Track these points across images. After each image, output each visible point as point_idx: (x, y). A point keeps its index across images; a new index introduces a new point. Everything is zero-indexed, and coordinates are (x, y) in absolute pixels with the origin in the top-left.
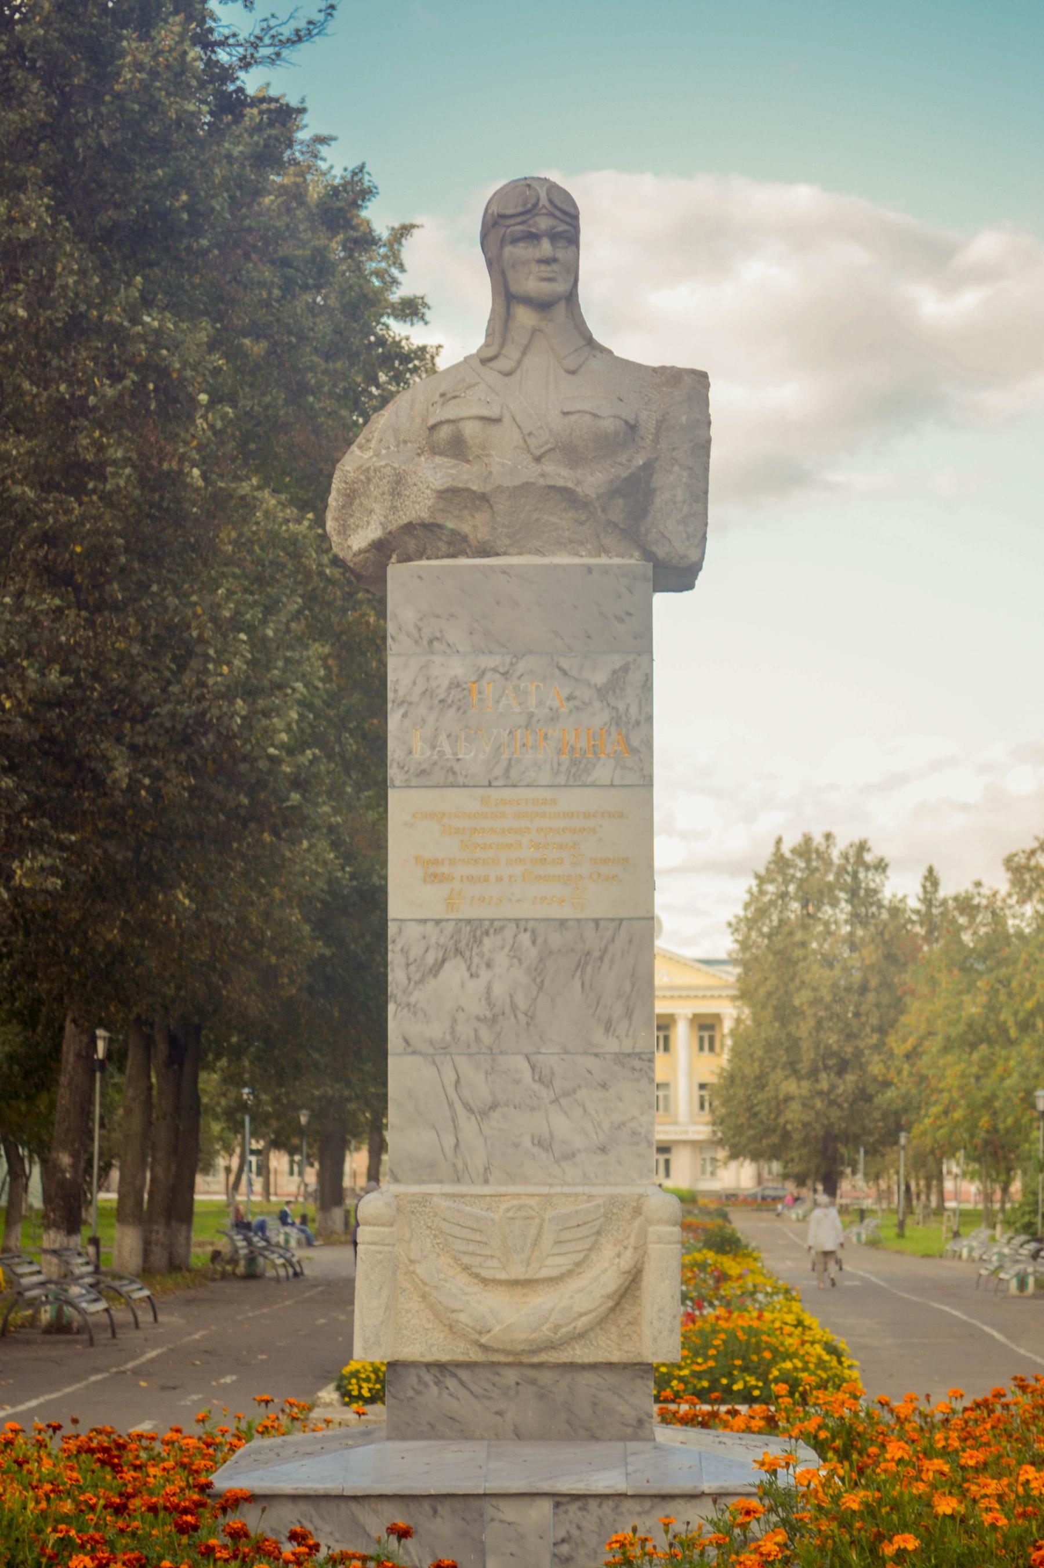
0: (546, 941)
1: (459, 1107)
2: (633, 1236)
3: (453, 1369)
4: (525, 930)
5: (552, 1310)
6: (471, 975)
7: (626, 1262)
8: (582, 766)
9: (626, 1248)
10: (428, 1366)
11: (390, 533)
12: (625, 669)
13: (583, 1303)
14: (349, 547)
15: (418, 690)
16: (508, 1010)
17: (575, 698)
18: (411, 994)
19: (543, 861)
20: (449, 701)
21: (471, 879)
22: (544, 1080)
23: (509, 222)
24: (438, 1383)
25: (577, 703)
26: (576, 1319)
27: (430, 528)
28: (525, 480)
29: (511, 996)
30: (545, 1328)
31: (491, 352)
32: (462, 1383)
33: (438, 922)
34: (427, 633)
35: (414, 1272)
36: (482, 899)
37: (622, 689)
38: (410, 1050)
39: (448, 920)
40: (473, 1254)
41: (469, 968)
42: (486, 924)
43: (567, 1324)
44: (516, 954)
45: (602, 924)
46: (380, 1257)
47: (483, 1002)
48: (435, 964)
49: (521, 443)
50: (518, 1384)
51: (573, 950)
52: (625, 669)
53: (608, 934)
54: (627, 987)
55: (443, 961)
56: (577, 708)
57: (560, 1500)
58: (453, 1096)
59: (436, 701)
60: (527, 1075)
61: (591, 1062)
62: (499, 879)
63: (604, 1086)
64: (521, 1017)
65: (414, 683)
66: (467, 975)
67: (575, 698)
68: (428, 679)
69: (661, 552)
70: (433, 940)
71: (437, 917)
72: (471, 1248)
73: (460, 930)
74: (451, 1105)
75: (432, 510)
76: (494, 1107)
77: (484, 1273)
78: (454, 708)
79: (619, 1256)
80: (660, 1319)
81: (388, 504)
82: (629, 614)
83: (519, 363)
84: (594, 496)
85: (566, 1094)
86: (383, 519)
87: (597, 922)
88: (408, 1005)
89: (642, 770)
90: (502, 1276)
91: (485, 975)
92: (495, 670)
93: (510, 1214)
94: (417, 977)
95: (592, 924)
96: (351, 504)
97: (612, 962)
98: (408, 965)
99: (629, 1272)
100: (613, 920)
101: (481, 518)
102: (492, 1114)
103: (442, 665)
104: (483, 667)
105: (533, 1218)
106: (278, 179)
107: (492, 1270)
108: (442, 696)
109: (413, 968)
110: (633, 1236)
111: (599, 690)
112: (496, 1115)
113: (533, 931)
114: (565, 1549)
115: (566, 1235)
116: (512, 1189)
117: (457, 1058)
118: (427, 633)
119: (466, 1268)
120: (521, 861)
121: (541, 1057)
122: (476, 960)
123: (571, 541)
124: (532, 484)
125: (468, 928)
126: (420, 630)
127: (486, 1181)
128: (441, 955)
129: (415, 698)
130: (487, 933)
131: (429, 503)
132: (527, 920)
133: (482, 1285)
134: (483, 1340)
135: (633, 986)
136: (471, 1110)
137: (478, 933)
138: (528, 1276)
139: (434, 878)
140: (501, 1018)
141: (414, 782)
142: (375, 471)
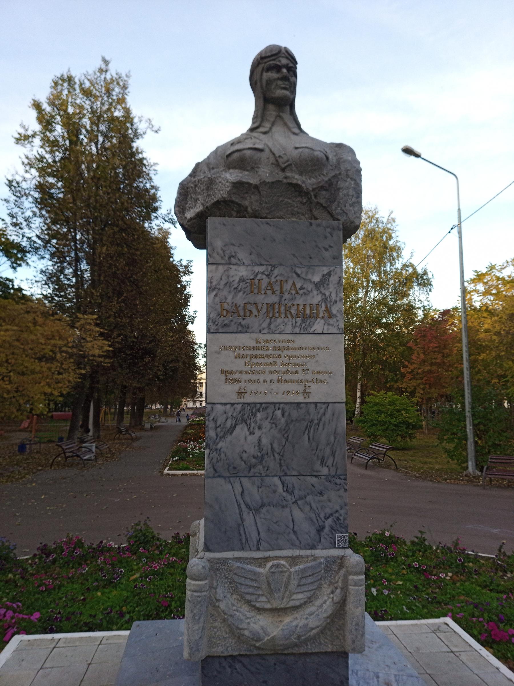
0: (289, 414)
1: (243, 506)
2: (340, 581)
3: (239, 658)
4: (279, 409)
5: (297, 626)
6: (250, 433)
7: (337, 596)
8: (307, 323)
9: (336, 588)
10: (225, 657)
11: (207, 207)
12: (329, 274)
13: (313, 622)
14: (186, 218)
15: (223, 282)
16: (270, 452)
17: (304, 289)
18: (218, 444)
19: (288, 372)
20: (239, 289)
21: (250, 381)
22: (289, 491)
23: (265, 61)
25: (304, 291)
26: (310, 631)
28: (277, 179)
29: (271, 444)
30: (293, 637)
31: (256, 125)
32: (244, 666)
33: (233, 404)
34: (228, 252)
35: (218, 606)
37: (328, 285)
38: (216, 475)
39: (238, 403)
40: (252, 594)
41: (249, 430)
42: (258, 405)
43: (305, 635)
44: (274, 422)
45: (319, 405)
46: (200, 599)
47: (257, 448)
48: (231, 427)
49: (274, 162)
50: (275, 664)
51: (304, 419)
52: (329, 274)
53: (322, 411)
54: (332, 439)
56: (305, 294)
59: (232, 289)
63: (321, 494)
64: (277, 455)
65: (221, 279)
66: (248, 433)
67: (304, 289)
68: (228, 277)
70: (230, 414)
71: (232, 402)
72: (251, 590)
73: (244, 409)
74: (239, 506)
76: (262, 506)
77: (258, 605)
78: (242, 292)
79: (332, 592)
80: (356, 630)
81: (205, 194)
82: (331, 247)
83: (270, 129)
84: (311, 189)
86: (202, 202)
87: (316, 404)
88: (216, 449)
89: (338, 326)
90: (268, 606)
91: (258, 433)
92: (263, 273)
93: (272, 570)
94: (222, 434)
95: (313, 406)
96: (186, 198)
97: (324, 425)
98: (216, 428)
99: (338, 603)
100: (324, 403)
102: (261, 510)
103: (236, 270)
104: (257, 271)
105: (285, 572)
106: (190, 405)
107: (262, 602)
108: (235, 286)
109: (219, 430)
110: (340, 581)
112: (264, 510)
113: (283, 409)
115: (304, 581)
116: (273, 553)
117: (242, 479)
118: (228, 252)
119: (248, 602)
120: (276, 372)
121: (287, 478)
122: (253, 425)
123: (298, 213)
124: (281, 181)
125: (249, 408)
126: (224, 251)
127: (258, 549)
128: (234, 422)
129: (221, 287)
130: (258, 410)
131: (228, 189)
132: (280, 403)
133: (256, 611)
134: (258, 645)
135: (335, 439)
136: (250, 509)
137: (254, 410)
138: (282, 606)
140: (266, 456)
141: (220, 331)
142: (198, 181)
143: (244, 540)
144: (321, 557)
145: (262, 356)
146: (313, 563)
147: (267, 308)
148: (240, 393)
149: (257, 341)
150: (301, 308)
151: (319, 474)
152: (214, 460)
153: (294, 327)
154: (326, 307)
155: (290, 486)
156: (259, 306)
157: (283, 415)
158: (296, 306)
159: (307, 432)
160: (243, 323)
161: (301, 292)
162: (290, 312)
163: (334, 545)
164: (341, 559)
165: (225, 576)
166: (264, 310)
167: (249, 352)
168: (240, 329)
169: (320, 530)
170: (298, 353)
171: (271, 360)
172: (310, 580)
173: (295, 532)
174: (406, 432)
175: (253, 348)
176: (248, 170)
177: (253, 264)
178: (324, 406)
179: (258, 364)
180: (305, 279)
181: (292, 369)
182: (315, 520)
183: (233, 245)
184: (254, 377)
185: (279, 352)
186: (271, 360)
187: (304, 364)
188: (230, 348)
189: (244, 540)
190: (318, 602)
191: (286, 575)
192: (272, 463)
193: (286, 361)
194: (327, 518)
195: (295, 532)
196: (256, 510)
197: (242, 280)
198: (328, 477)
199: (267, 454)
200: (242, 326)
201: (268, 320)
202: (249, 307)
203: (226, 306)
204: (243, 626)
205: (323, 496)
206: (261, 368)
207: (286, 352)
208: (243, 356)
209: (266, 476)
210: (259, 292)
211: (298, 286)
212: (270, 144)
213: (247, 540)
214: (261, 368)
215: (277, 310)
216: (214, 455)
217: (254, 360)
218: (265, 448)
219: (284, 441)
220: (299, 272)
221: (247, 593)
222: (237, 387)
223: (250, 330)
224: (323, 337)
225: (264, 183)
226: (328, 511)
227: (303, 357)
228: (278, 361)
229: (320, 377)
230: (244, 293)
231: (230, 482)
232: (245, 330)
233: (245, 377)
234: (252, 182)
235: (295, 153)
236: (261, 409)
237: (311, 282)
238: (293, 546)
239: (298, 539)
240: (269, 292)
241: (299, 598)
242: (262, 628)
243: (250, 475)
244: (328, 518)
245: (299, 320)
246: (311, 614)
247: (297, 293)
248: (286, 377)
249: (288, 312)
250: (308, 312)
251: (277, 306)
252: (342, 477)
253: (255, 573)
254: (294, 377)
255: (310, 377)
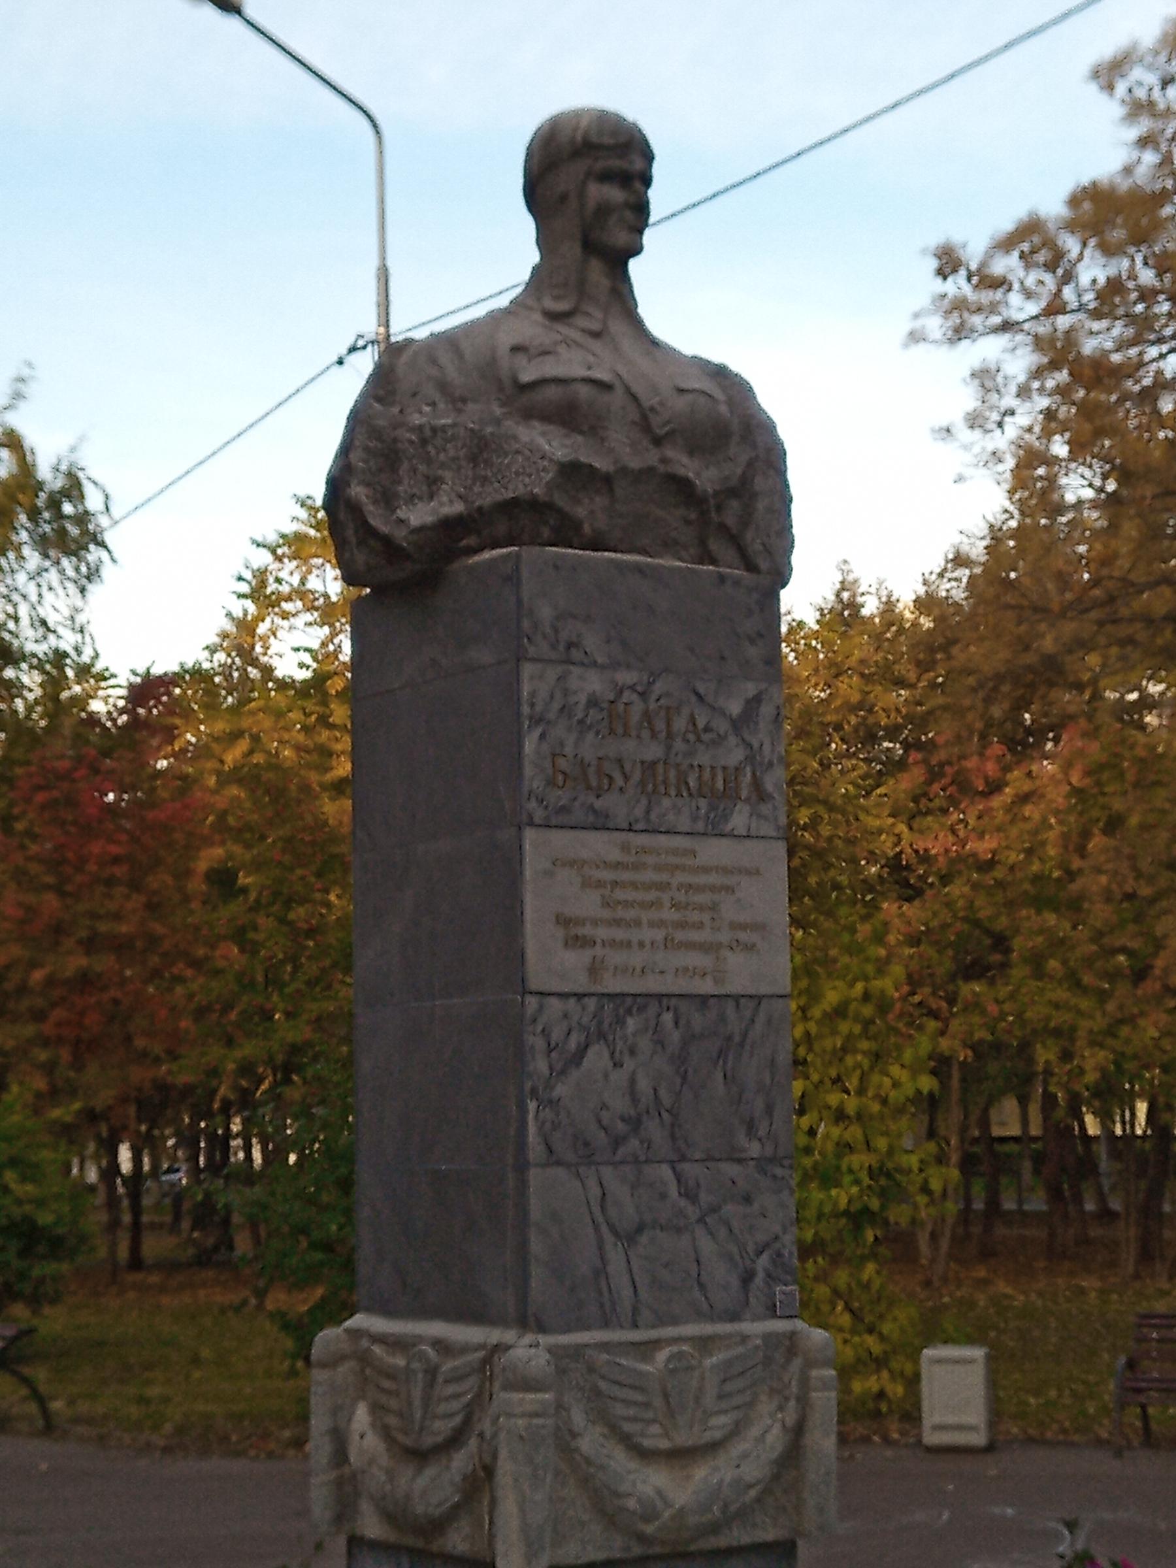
2: (794, 1383)
4: (668, 1009)
6: (615, 1065)
7: (790, 1416)
9: (787, 1399)
12: (757, 699)
15: (556, 706)
19: (682, 925)
21: (613, 944)
22: (689, 1194)
27: (534, 506)
29: (655, 1090)
33: (580, 996)
34: (564, 636)
41: (612, 1054)
45: (743, 1001)
53: (748, 1014)
55: (587, 1046)
58: (600, 1219)
62: (641, 945)
64: (665, 1115)
65: (552, 697)
70: (576, 1018)
71: (581, 990)
75: (549, 486)
76: (640, 1229)
77: (647, 1443)
90: (664, 1444)
91: (629, 1064)
92: (632, 688)
94: (558, 1067)
101: (600, 501)
107: (654, 1439)
108: (580, 715)
112: (644, 1239)
113: (676, 1011)
115: (728, 1387)
117: (601, 1168)
120: (661, 924)
122: (620, 1045)
126: (556, 631)
127: (635, 1326)
128: (583, 1038)
129: (551, 716)
130: (629, 1012)
139: (577, 942)
141: (554, 822)
143: (608, 1305)
144: (757, 1336)
145: (634, 885)
146: (740, 1350)
147: (643, 773)
148: (594, 970)
149: (625, 848)
150: (707, 775)
151: (743, 1155)
152: (548, 1125)
153: (695, 819)
154: (754, 774)
155: (691, 1183)
156: (628, 767)
157: (676, 1023)
158: (697, 769)
159: (721, 1062)
160: (598, 804)
161: (706, 737)
162: (687, 783)
163: (772, 1311)
164: (791, 1338)
165: (578, 1384)
166: (637, 776)
167: (607, 875)
168: (591, 818)
169: (747, 1278)
170: (702, 879)
171: (651, 896)
172: (740, 1383)
173: (702, 1286)
174: (22, 1276)
175: (617, 866)
176: (581, 433)
177: (615, 665)
178: (752, 1004)
179: (627, 904)
180: (713, 708)
181: (695, 916)
182: (737, 1257)
183: (574, 617)
184: (620, 934)
185: (664, 877)
186: (651, 896)
187: (714, 907)
188: (572, 863)
189: (608, 1305)
190: (755, 1431)
191: (696, 1374)
192: (654, 1130)
193: (681, 897)
194: (759, 1253)
195: (702, 1286)
196: (629, 1238)
197: (593, 702)
198: (763, 1164)
199: (648, 1112)
200: (595, 812)
201: (644, 801)
202: (608, 767)
203: (562, 763)
204: (624, 1487)
205: (751, 1205)
206: (631, 914)
207: (681, 878)
208: (600, 884)
209: (646, 1161)
210: (626, 734)
211: (701, 724)
212: (622, 370)
213: (613, 1303)
214: (631, 914)
215: (660, 778)
216: (547, 1114)
217: (620, 895)
218: (643, 1100)
219: (678, 1081)
220: (702, 691)
221: (628, 1419)
222: (586, 956)
223: (611, 825)
224: (749, 843)
225: (624, 471)
226: (761, 1237)
227: (713, 889)
228: (666, 898)
229: (743, 936)
230: (597, 733)
231: (578, 1175)
232: (601, 823)
233: (602, 933)
234: (597, 465)
235: (681, 404)
236: (635, 1010)
237: (725, 714)
238: (699, 1316)
239: (706, 1298)
240: (645, 734)
241: (721, 1422)
242: (659, 1492)
243: (618, 1158)
244: (762, 1252)
245: (703, 803)
246: (745, 1456)
247: (699, 740)
248: (680, 936)
249: (683, 788)
250: (720, 784)
251: (660, 769)
252: (786, 1162)
253: (641, 1374)
254: (695, 936)
255: (724, 937)
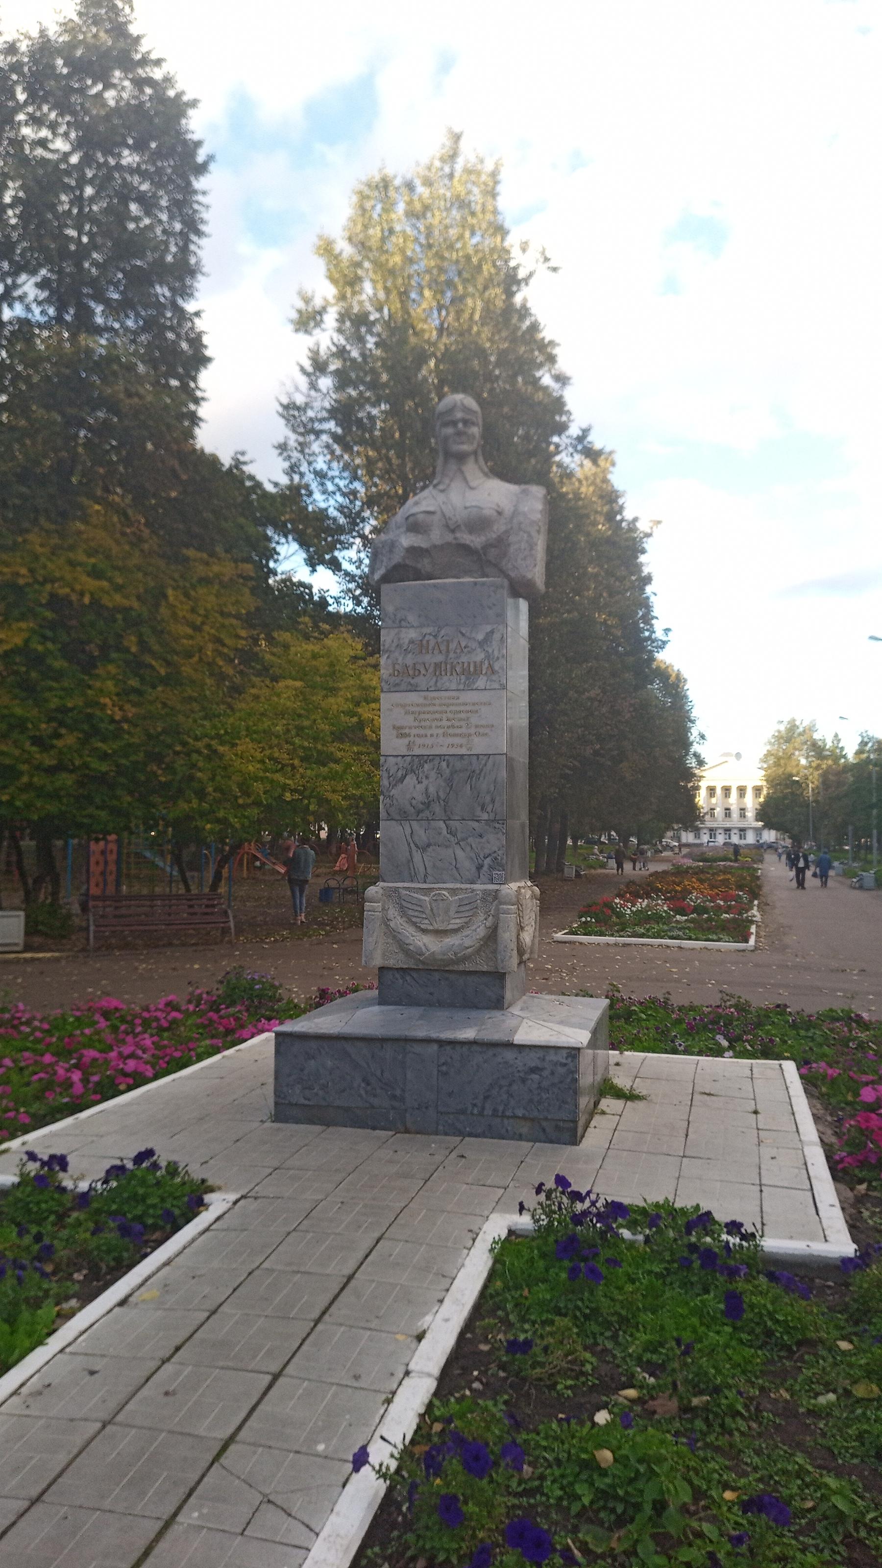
1: (412, 845)
12: (492, 632)
15: (394, 645)
19: (453, 727)
21: (418, 736)
24: (402, 978)
33: (403, 756)
36: (453, 745)
44: (440, 773)
52: (492, 632)
57: (441, 1043)
60: (445, 831)
61: (475, 825)
69: (513, 574)
72: (416, 914)
74: (409, 844)
76: (429, 845)
77: (422, 926)
85: (463, 840)
87: (478, 755)
91: (425, 782)
111: (479, 643)
112: (430, 849)
114: (444, 1068)
115: (462, 909)
116: (436, 886)
127: (425, 882)
